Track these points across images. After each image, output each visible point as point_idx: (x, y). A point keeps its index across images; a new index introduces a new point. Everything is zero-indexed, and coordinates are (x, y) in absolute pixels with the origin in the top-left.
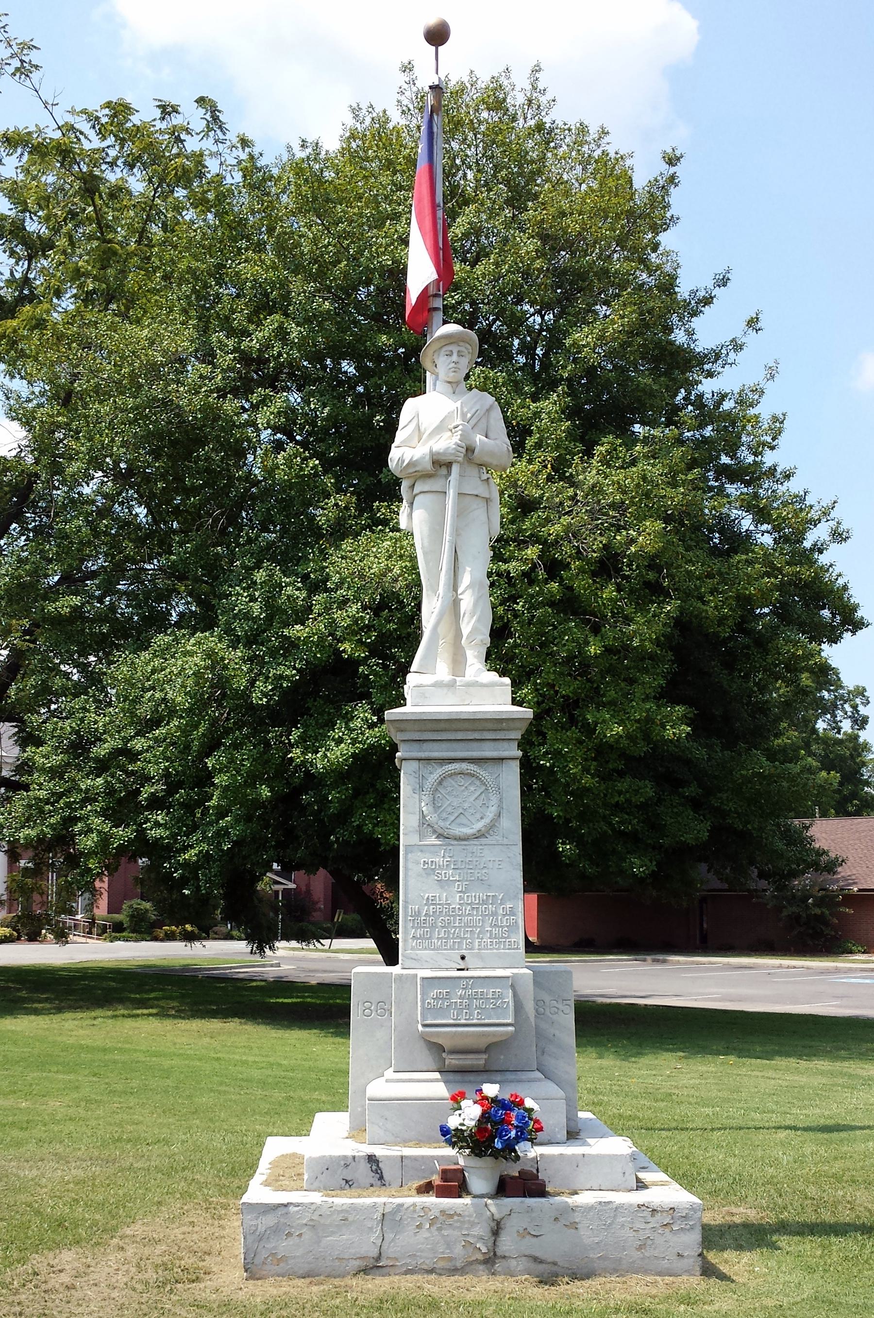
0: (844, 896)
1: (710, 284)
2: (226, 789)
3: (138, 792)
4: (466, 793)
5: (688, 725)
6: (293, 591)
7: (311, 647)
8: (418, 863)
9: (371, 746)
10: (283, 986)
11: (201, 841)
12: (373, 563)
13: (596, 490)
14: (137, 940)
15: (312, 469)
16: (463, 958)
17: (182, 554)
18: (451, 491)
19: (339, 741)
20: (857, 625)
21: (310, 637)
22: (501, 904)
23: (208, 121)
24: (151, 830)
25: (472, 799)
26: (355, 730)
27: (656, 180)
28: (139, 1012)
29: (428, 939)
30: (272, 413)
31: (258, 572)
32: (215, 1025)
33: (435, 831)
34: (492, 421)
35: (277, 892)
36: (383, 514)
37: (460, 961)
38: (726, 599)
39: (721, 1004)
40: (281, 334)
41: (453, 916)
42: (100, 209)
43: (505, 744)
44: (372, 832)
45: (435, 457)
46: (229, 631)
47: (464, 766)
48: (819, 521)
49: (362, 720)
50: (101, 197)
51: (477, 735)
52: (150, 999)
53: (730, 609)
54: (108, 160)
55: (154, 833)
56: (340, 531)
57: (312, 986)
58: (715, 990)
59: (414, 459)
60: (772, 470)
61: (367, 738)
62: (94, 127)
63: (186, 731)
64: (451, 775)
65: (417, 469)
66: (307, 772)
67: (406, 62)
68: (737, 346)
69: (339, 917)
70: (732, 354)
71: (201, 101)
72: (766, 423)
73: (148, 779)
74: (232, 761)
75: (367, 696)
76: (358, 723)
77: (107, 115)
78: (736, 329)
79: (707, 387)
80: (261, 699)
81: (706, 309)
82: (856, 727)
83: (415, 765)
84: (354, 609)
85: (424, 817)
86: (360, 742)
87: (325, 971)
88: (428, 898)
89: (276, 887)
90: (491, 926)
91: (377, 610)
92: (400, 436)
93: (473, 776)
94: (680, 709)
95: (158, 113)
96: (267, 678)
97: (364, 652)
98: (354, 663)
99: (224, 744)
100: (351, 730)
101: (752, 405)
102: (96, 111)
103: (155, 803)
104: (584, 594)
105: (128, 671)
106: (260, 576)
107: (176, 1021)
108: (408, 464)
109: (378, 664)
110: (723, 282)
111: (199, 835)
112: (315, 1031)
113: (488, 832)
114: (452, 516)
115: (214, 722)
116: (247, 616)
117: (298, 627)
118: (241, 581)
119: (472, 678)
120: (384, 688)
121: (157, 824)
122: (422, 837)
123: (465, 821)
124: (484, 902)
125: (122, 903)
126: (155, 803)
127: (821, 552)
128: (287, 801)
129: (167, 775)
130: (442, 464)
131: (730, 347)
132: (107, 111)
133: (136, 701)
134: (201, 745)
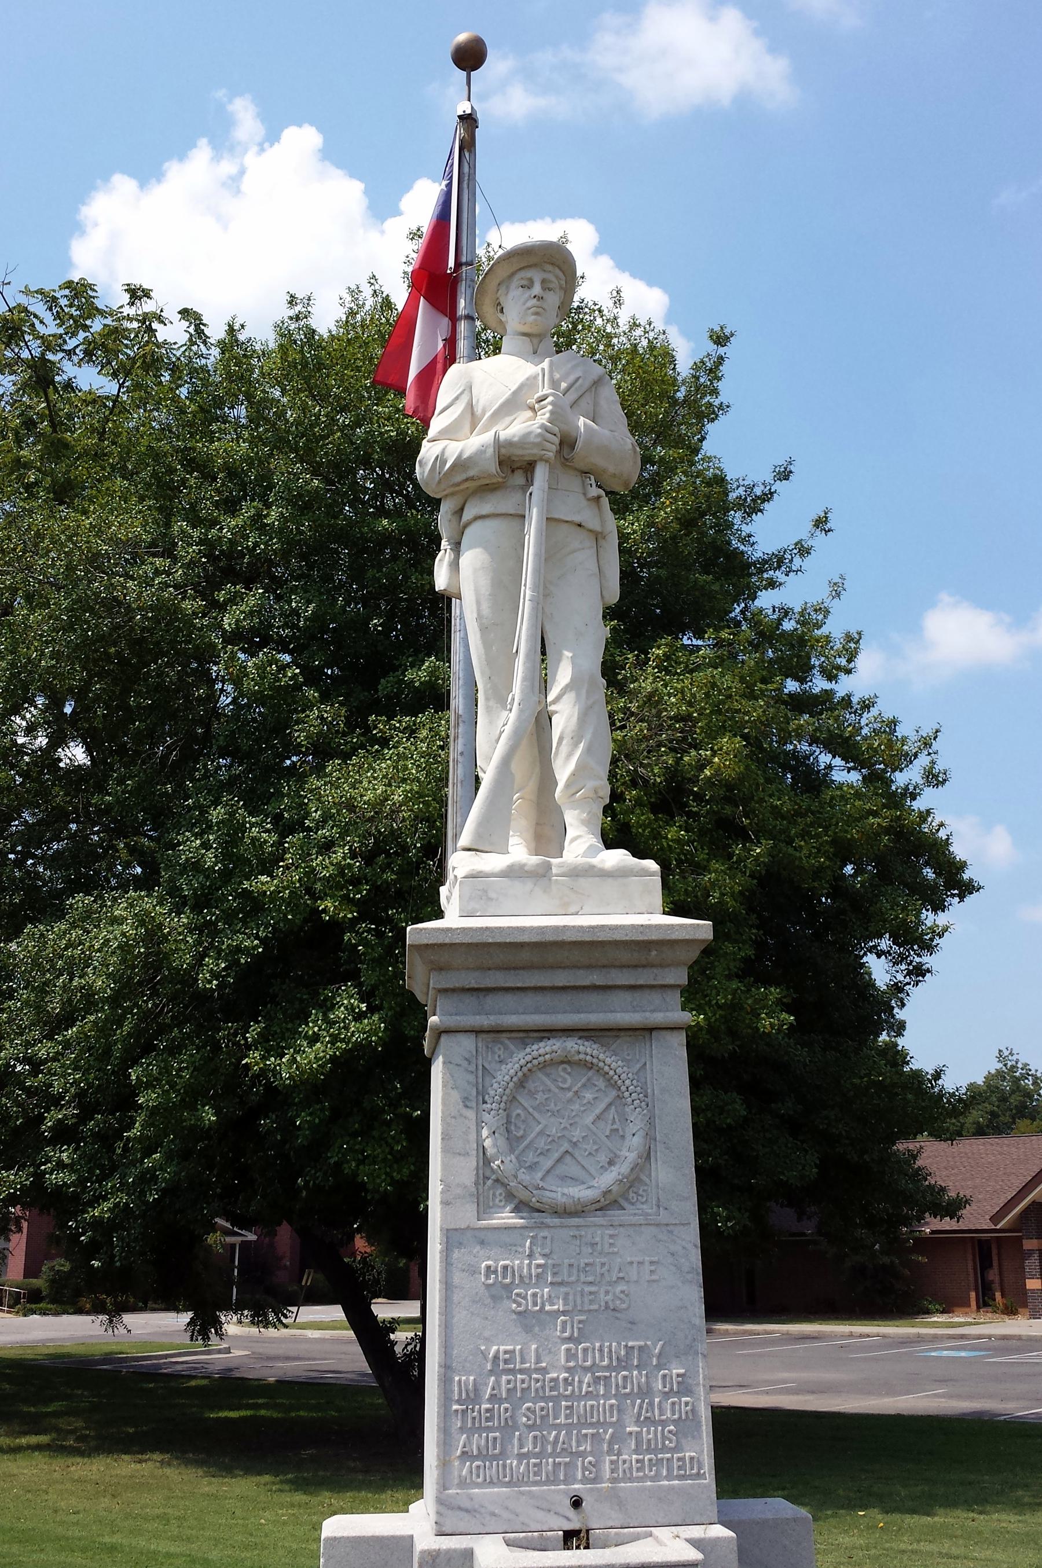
0: (915, 1239)
1: (769, 478)
2: (153, 1112)
3: (41, 1119)
4: (576, 1107)
5: (790, 1013)
6: (260, 832)
7: (280, 906)
8: (474, 1271)
9: (358, 1045)
10: (232, 1386)
11: (118, 1190)
12: (366, 790)
13: (653, 700)
14: (57, 1314)
15: (291, 679)
16: (577, 1503)
17: (119, 793)
18: (535, 511)
19: (314, 1039)
20: (967, 889)
21: (280, 892)
22: (659, 1367)
23: (191, 335)
24: (51, 1174)
25: (589, 1119)
26: (335, 1023)
27: (702, 362)
28: (24, 1441)
29: (495, 1457)
30: (242, 612)
31: (215, 809)
32: (125, 1467)
33: (510, 1196)
34: (603, 402)
35: (233, 1246)
36: (381, 731)
37: (571, 1513)
38: (821, 844)
39: (800, 1398)
40: (257, 520)
41: (551, 1398)
42: (55, 406)
43: (656, 997)
44: (355, 1174)
45: (503, 451)
46: (174, 891)
47: (572, 1045)
48: (916, 755)
49: (346, 1008)
50: (56, 390)
51: (595, 978)
52: (47, 1415)
53: (827, 858)
54: (65, 347)
55: (57, 1178)
56: (324, 750)
57: (269, 1385)
58: (785, 1375)
59: (465, 456)
60: (846, 702)
61: (353, 1035)
62: (51, 309)
63: (104, 1029)
64: (544, 1066)
65: (471, 473)
66: (268, 1086)
67: (414, 229)
68: (804, 551)
69: (307, 1280)
70: (797, 561)
71: (185, 313)
72: (838, 643)
73: (56, 1101)
74: (166, 1070)
75: (353, 976)
76: (341, 1013)
77: (66, 296)
78: (803, 530)
79: (766, 600)
80: (210, 982)
81: (766, 505)
82: (893, 1034)
83: (467, 1043)
84: (339, 854)
85: (487, 1161)
86: (342, 1041)
87: (288, 1358)
88: (496, 1357)
89: (230, 1239)
90: (637, 1422)
91: (369, 858)
92: (437, 424)
93: (590, 1066)
94: (775, 992)
95: (126, 298)
96: (219, 951)
97: (352, 913)
98: (337, 927)
99: (155, 1048)
100: (331, 1023)
101: (819, 627)
102: (54, 291)
103: (63, 1134)
104: (642, 835)
105: (34, 947)
106: (216, 814)
107: (70, 1460)
108: (454, 466)
109: (369, 931)
110: (784, 475)
111: (115, 1181)
112: (267, 1478)
113: (624, 1195)
114: (537, 555)
115: (146, 1016)
116: (196, 866)
117: (264, 878)
118: (194, 825)
119: (581, 860)
120: (379, 962)
121: (61, 1165)
122: (484, 1209)
123: (574, 1170)
124: (623, 1363)
125: (42, 1264)
126: (63, 1134)
127: (914, 797)
128: (239, 1127)
129: (81, 1095)
130: (514, 465)
131: (795, 551)
132: (67, 292)
133: (43, 991)
134: (125, 1050)
